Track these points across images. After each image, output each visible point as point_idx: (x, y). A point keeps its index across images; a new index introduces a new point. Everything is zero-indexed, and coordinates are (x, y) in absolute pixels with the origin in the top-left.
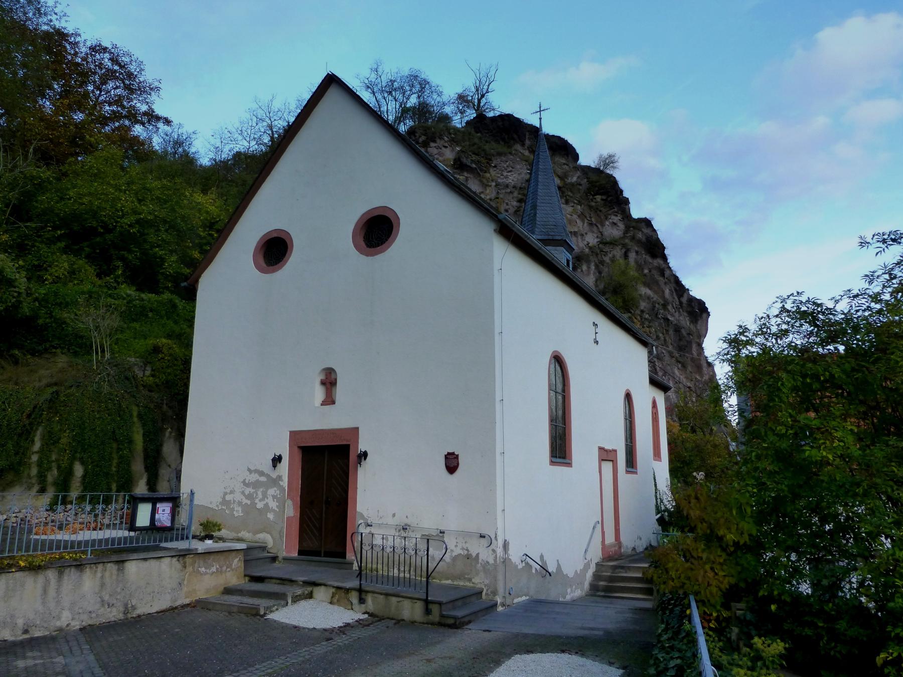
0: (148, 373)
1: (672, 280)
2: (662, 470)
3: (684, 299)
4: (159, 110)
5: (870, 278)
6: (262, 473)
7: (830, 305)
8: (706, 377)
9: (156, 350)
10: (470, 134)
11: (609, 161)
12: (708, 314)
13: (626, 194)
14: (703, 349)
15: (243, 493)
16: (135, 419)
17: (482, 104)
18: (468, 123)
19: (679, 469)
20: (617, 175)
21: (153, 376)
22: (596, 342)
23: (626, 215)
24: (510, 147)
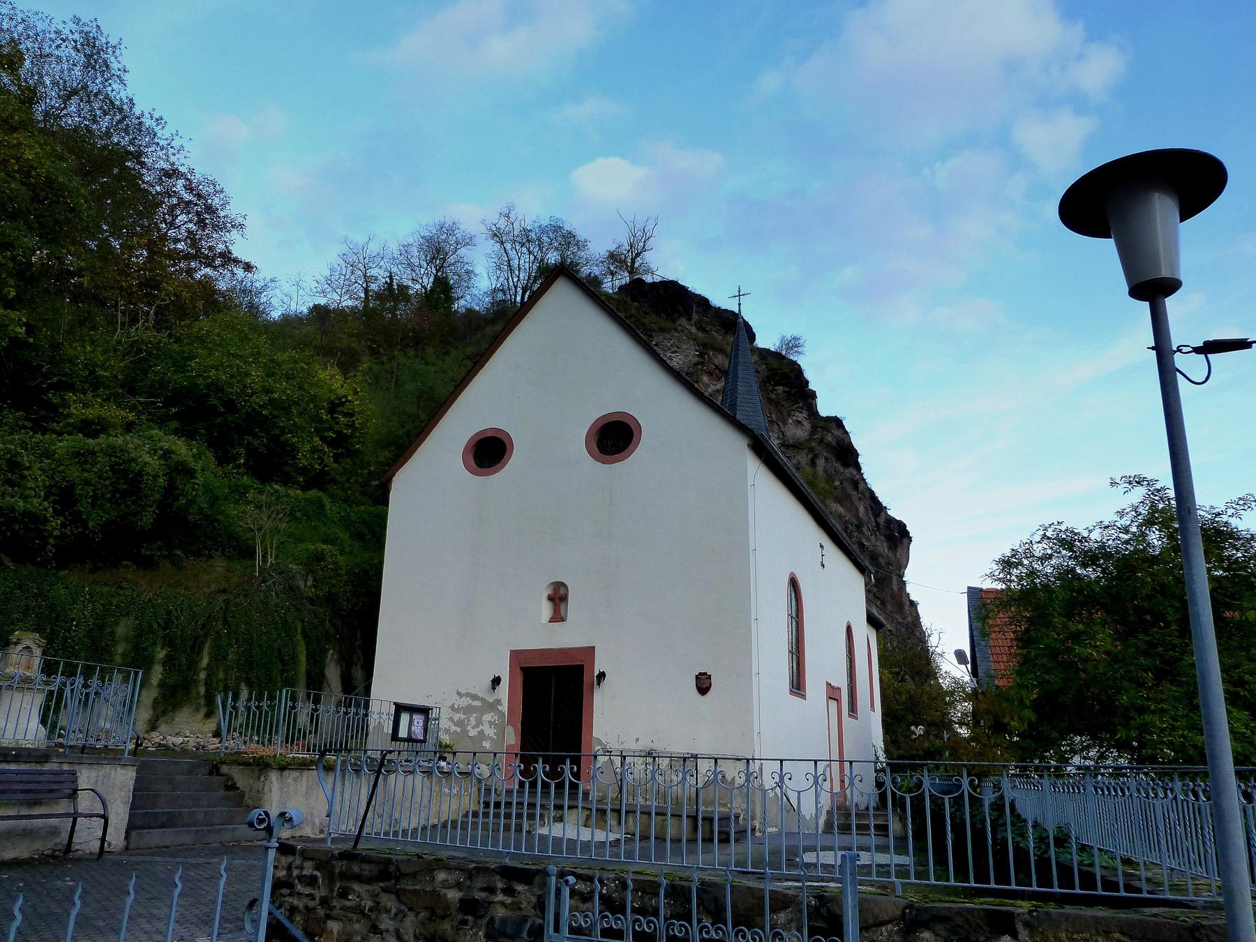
0: (309, 583)
1: (867, 495)
2: (877, 717)
3: (882, 520)
4: (237, 252)
5: (1121, 514)
6: (475, 697)
7: (1085, 535)
8: (909, 619)
9: (319, 557)
10: (626, 303)
11: (794, 344)
12: (910, 539)
13: (811, 387)
14: (904, 583)
15: (451, 719)
16: (299, 637)
17: (636, 265)
18: (621, 288)
19: (892, 721)
20: (802, 361)
21: (315, 587)
22: (823, 566)
24: (673, 321)
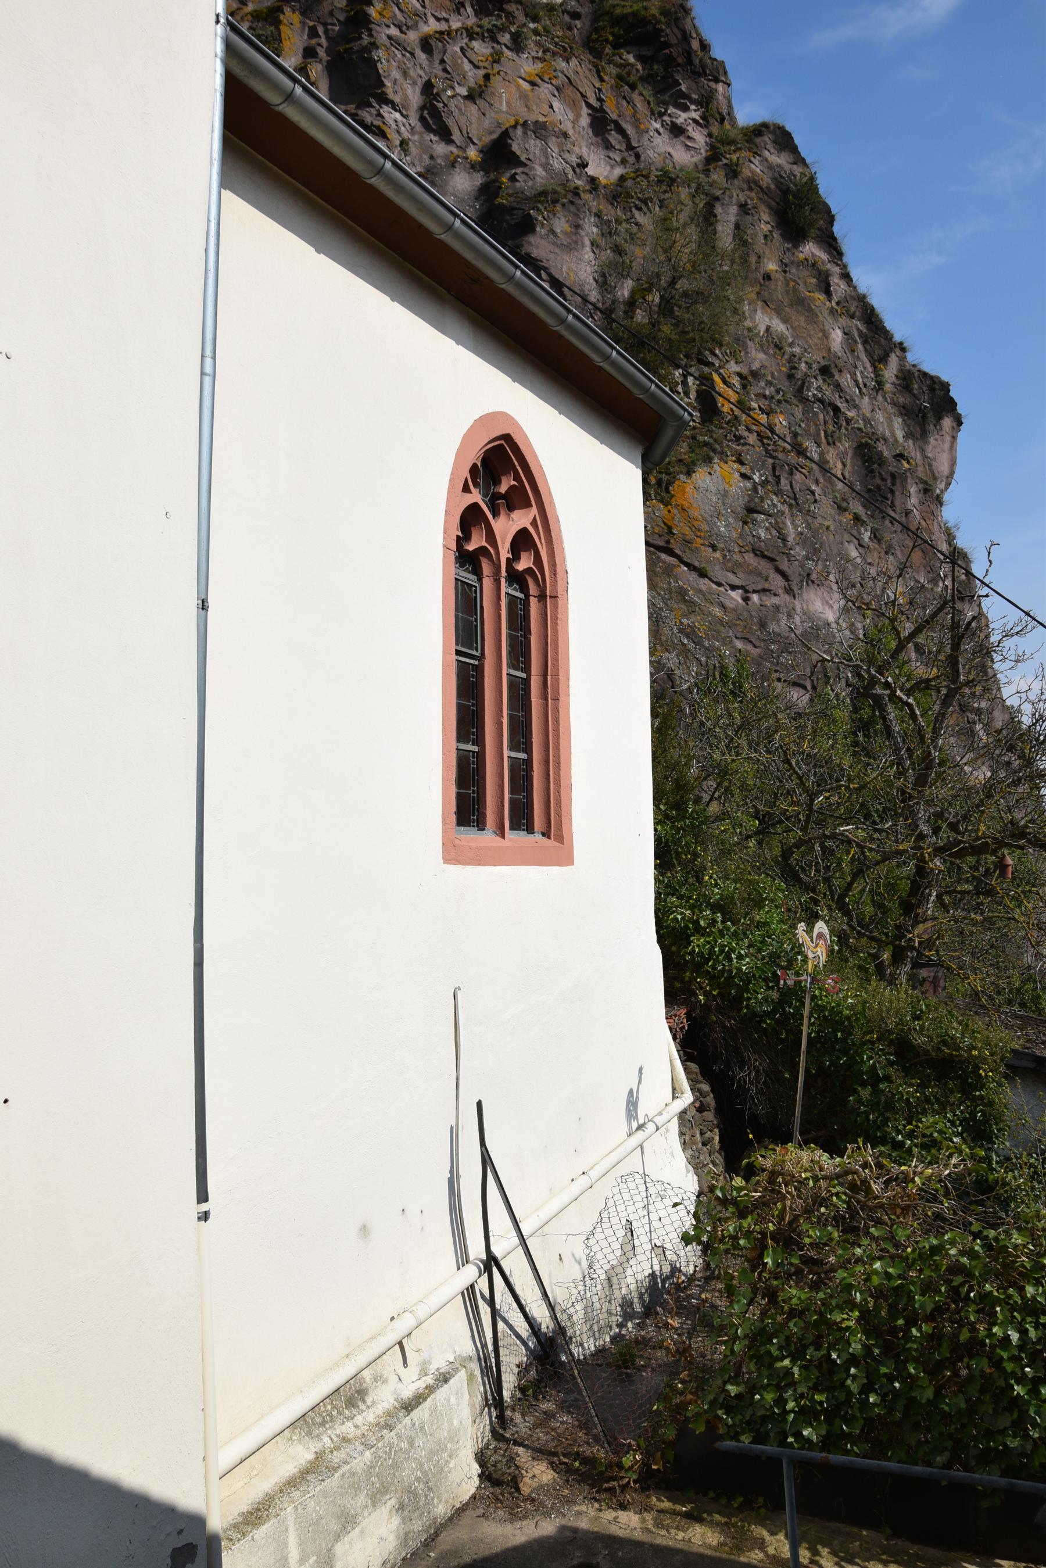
23: (715, 116)
